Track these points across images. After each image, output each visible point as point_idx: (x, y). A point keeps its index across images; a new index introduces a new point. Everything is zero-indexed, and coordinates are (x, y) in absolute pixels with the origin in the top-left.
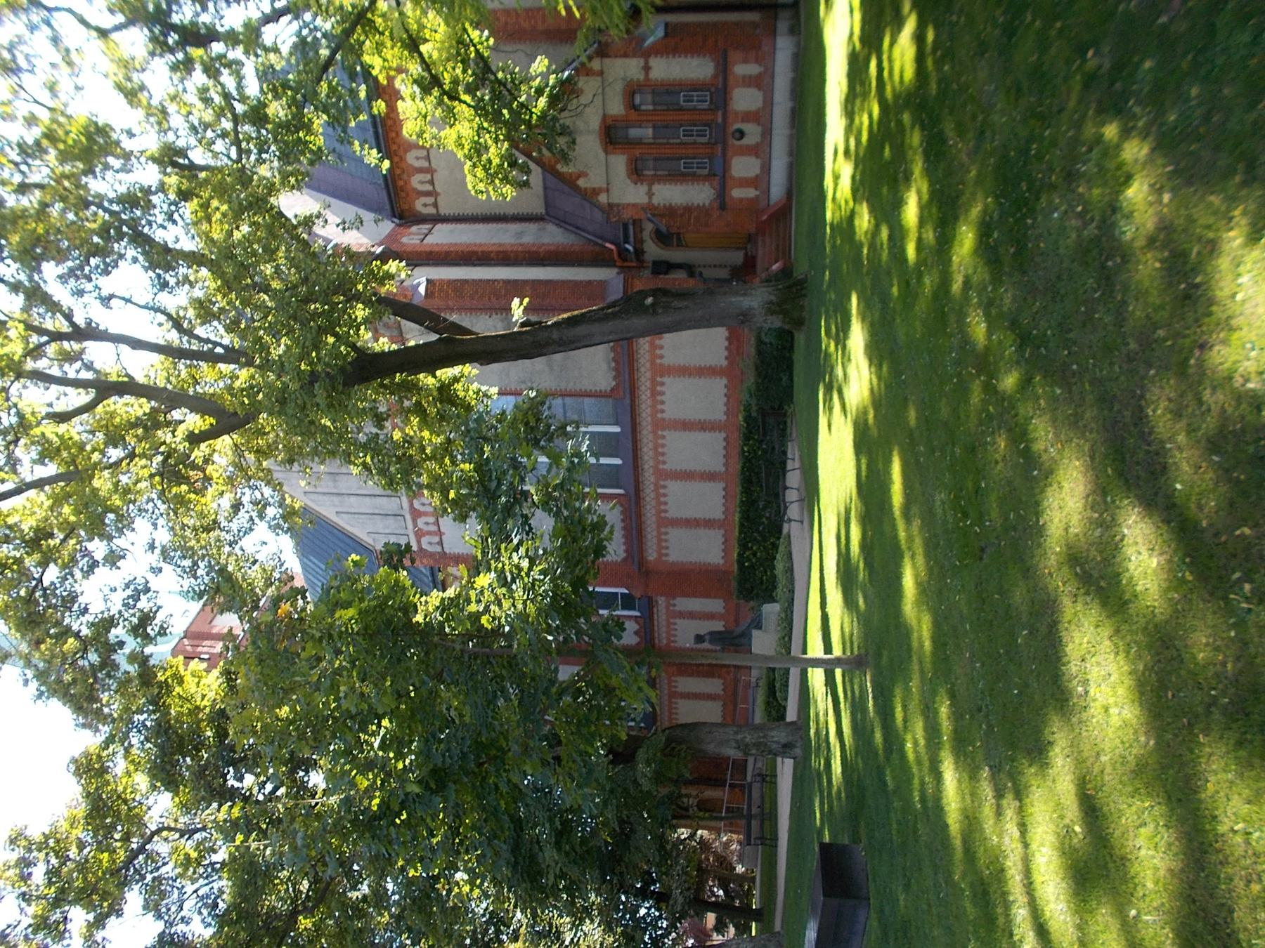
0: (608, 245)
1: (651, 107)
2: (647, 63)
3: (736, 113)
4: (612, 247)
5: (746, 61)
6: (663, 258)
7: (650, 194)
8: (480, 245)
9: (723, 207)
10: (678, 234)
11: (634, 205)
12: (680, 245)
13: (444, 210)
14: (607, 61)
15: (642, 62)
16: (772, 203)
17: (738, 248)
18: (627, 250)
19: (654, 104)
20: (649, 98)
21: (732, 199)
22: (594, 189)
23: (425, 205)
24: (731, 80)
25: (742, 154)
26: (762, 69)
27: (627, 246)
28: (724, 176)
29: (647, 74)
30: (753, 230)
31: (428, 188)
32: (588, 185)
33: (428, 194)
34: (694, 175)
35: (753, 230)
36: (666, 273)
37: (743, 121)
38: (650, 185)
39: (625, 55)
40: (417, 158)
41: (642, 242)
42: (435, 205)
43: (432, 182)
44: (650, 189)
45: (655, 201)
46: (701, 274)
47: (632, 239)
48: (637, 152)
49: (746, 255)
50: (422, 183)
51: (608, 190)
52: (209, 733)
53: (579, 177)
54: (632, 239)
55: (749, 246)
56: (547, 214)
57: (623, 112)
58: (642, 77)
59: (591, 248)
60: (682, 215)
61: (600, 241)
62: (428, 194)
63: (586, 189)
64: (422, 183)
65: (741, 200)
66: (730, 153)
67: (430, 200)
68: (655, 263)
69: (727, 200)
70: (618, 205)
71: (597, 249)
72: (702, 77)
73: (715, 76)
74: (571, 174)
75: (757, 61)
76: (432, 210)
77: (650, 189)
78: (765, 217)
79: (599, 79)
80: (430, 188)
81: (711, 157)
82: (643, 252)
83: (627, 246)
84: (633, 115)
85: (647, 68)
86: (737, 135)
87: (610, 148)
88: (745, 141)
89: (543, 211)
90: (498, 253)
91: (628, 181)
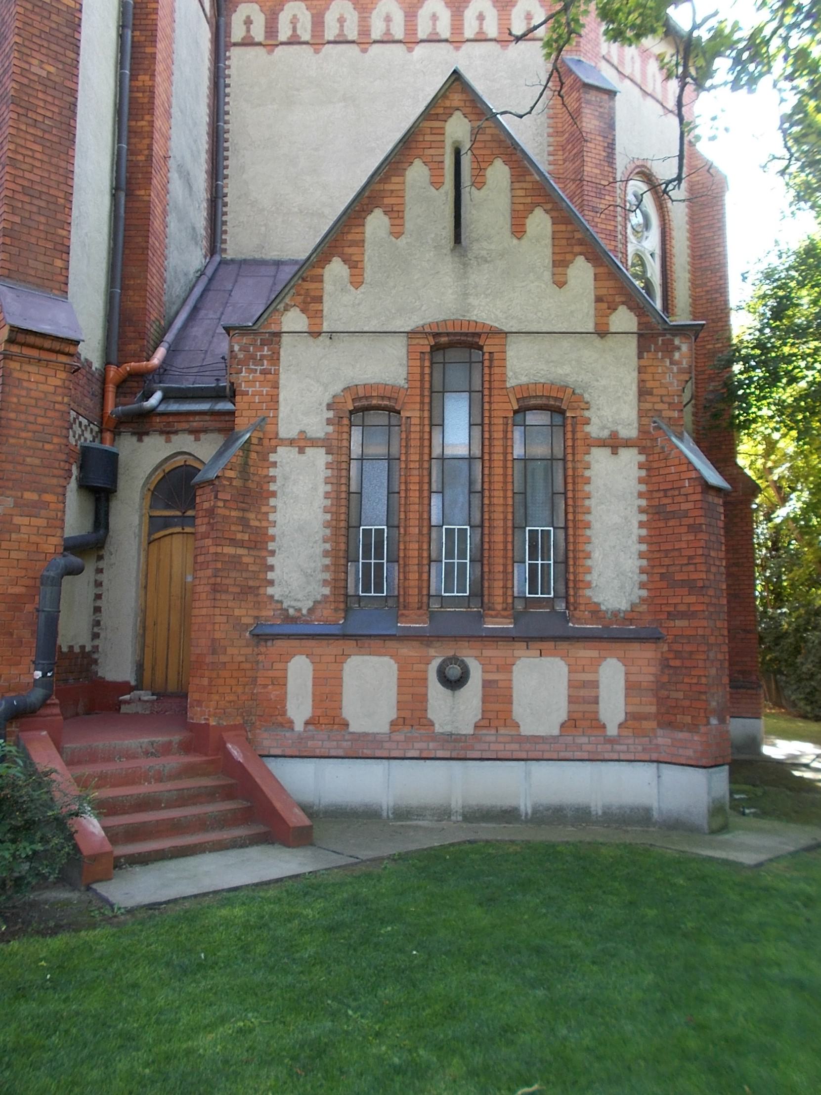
0: (161, 352)
1: (518, 451)
2: (628, 444)
3: (507, 668)
4: (157, 359)
5: (631, 688)
6: (122, 483)
7: (302, 443)
8: (170, 53)
9: (261, 637)
10: (185, 521)
11: (274, 400)
12: (156, 525)
13: (236, 57)
14: (632, 344)
15: (630, 431)
16: (274, 765)
17: (140, 667)
18: (148, 396)
19: (525, 460)
20: (540, 450)
21: (286, 658)
22: (319, 300)
23: (248, 22)
24: (585, 653)
25: (402, 683)
26: (612, 730)
27: (158, 396)
28: (345, 636)
29: (602, 443)
30: (198, 715)
31: (284, 34)
32: (328, 286)
33: (271, 29)
34: (351, 557)
35: (198, 715)
36: (84, 486)
37: (487, 684)
38: (326, 444)
39: (643, 393)
40: (341, 20)
41: (168, 433)
42: (248, 42)
43: (294, 41)
44: (314, 443)
45: (284, 455)
46: (75, 571)
47: (174, 407)
48: (412, 412)
49: (126, 687)
50: (294, 21)
51: (315, 334)
52: (389, 929)
53: (355, 265)
54: (174, 407)
55: (146, 696)
56: (223, 262)
57: (511, 383)
58: (594, 430)
59: (154, 315)
60: (244, 523)
61: (169, 337)
62: (271, 29)
63: (320, 279)
64: (294, 21)
65: (281, 682)
66: (407, 650)
67: (258, 32)
68: (112, 459)
69: (281, 645)
70: (275, 358)
71: (152, 330)
72: (593, 578)
73: (596, 612)
74: (360, 243)
75: (632, 718)
76: (237, 33)
77: (314, 443)
78: (236, 752)
79: (591, 327)
80: (284, 35)
81: (505, 609)
82: (140, 435)
83: (158, 396)
84: (504, 407)
85: (614, 444)
86: (454, 671)
87: (425, 344)
88: (435, 690)
89: (229, 256)
90: (151, 92)
91: (337, 388)
